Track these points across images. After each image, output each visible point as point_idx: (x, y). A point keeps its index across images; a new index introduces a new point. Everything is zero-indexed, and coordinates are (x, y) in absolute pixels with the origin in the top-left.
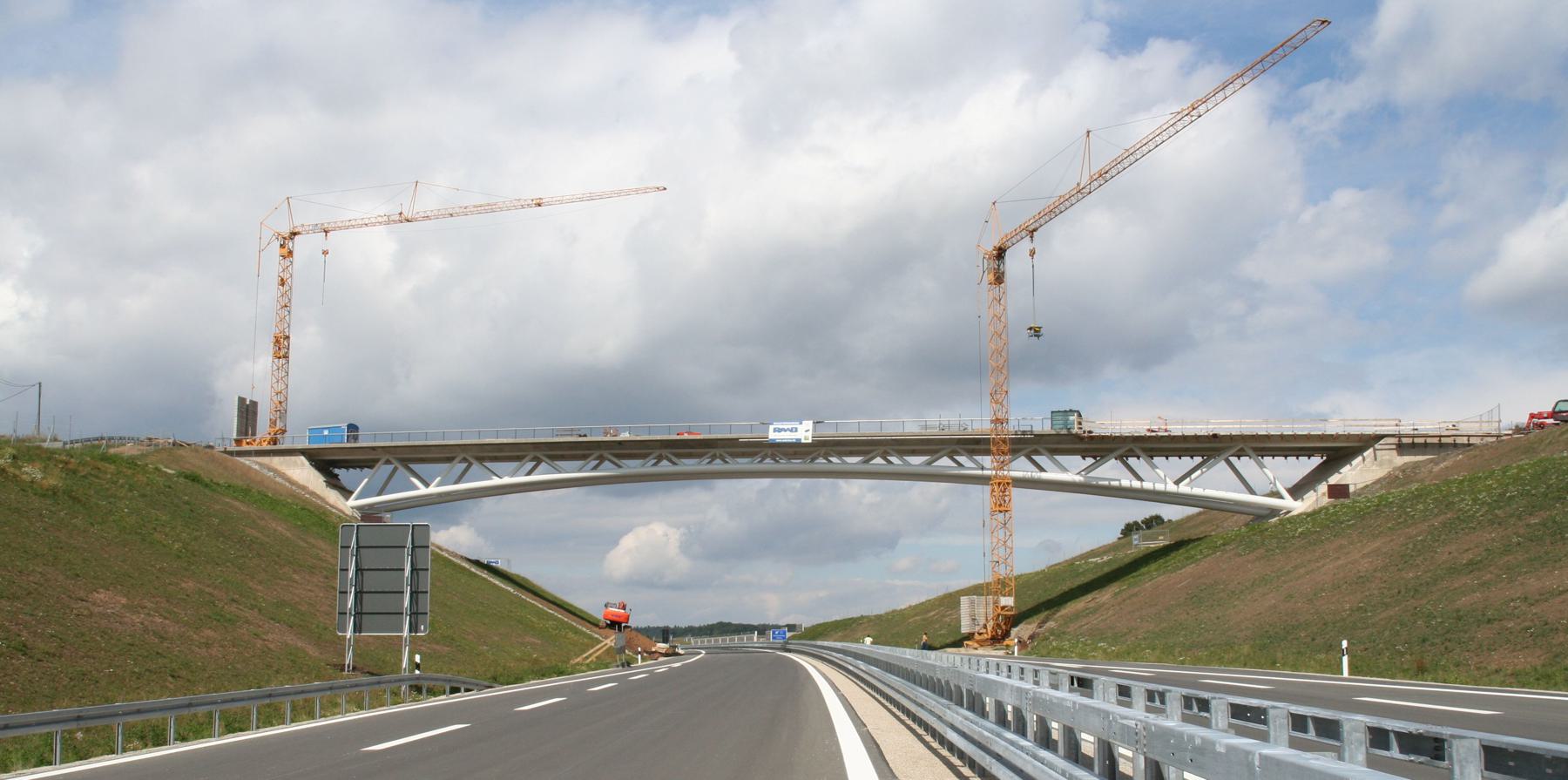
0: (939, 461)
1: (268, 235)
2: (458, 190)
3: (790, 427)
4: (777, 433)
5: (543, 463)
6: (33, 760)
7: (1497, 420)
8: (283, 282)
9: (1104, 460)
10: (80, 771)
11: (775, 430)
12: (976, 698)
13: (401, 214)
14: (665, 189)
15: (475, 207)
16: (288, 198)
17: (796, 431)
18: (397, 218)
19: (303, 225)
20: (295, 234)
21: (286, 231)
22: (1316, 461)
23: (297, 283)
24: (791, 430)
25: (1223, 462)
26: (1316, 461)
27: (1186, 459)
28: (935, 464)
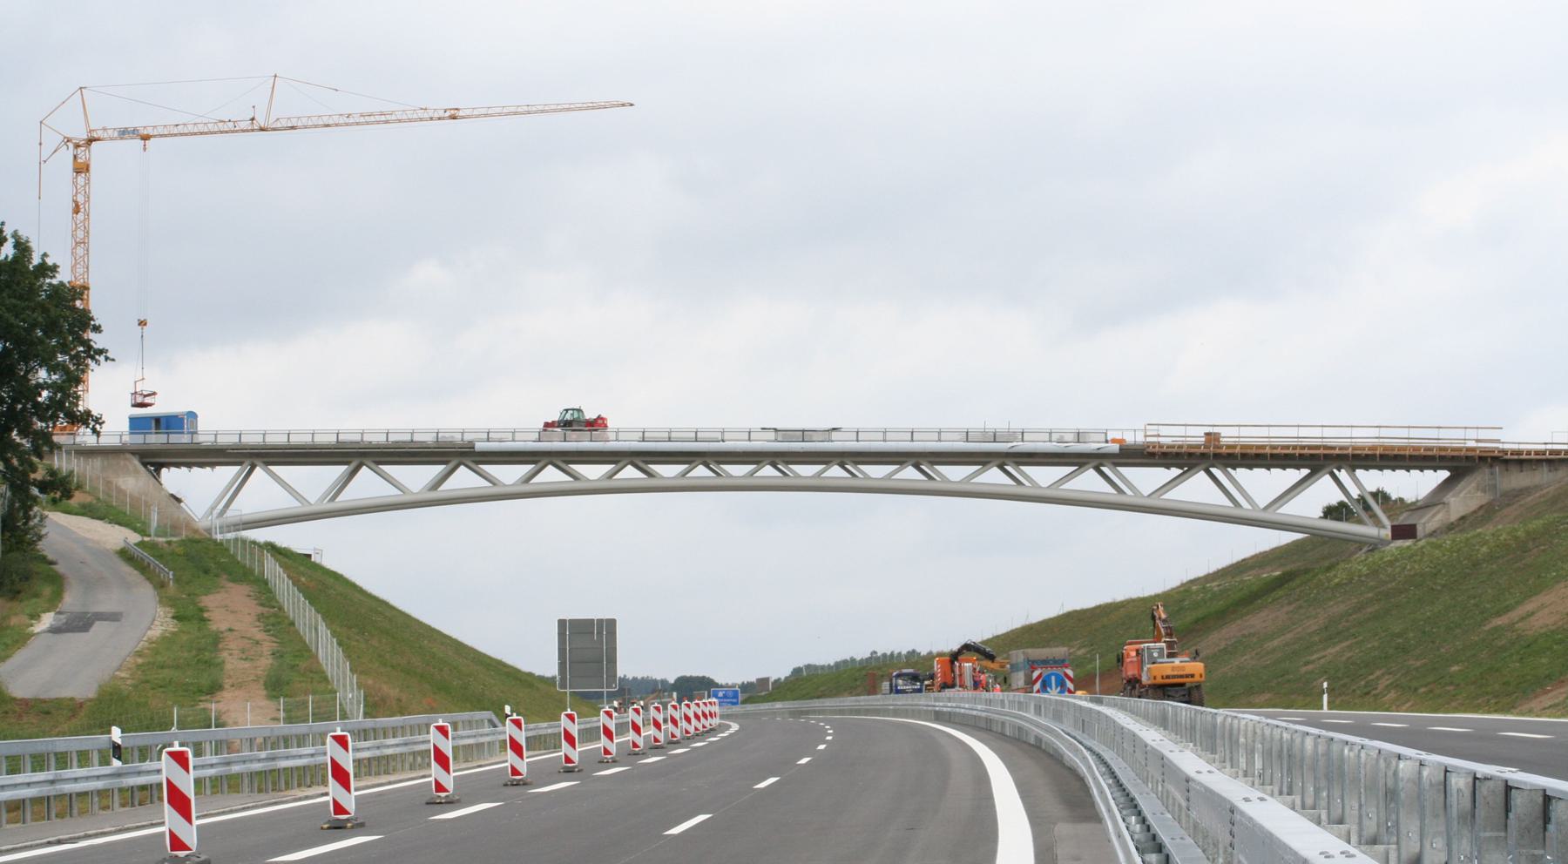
0: (692, 472)
1: (53, 141)
2: (337, 90)
5: (364, 467)
6: (1485, 793)
7: (725, 438)
8: (77, 210)
9: (1192, 472)
10: (44, 855)
12: (1189, 739)
13: (253, 119)
14: (632, 105)
15: (362, 115)
16: (81, 88)
18: (245, 125)
19: (105, 129)
20: (90, 141)
21: (83, 135)
22: (1444, 474)
23: (97, 207)
25: (1328, 476)
26: (1444, 474)
27: (1173, 469)
28: (615, 477)
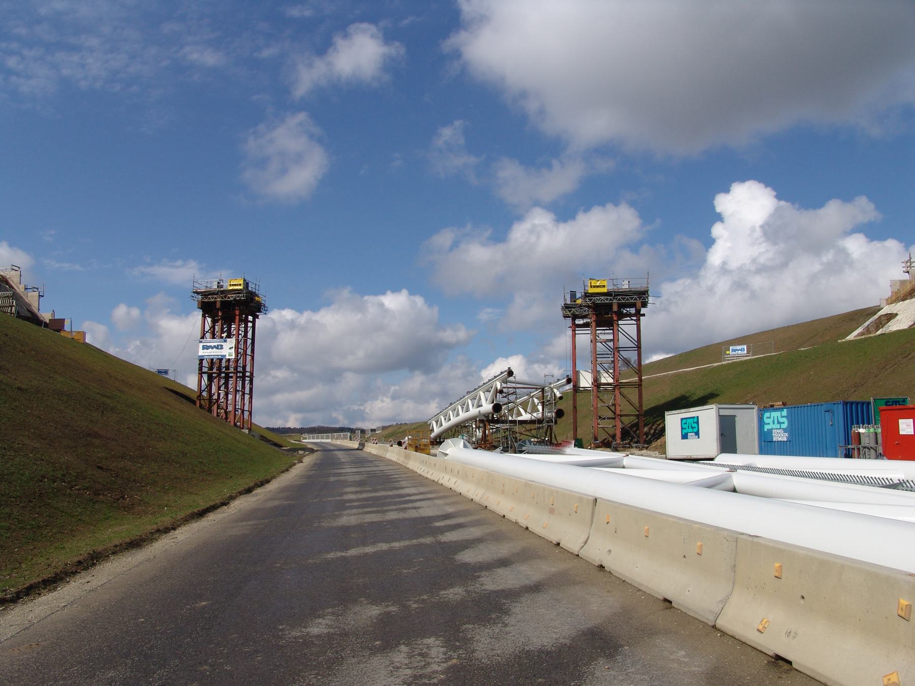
3: (216, 344)
4: (205, 351)
11: (204, 348)
17: (222, 348)
24: (217, 347)
